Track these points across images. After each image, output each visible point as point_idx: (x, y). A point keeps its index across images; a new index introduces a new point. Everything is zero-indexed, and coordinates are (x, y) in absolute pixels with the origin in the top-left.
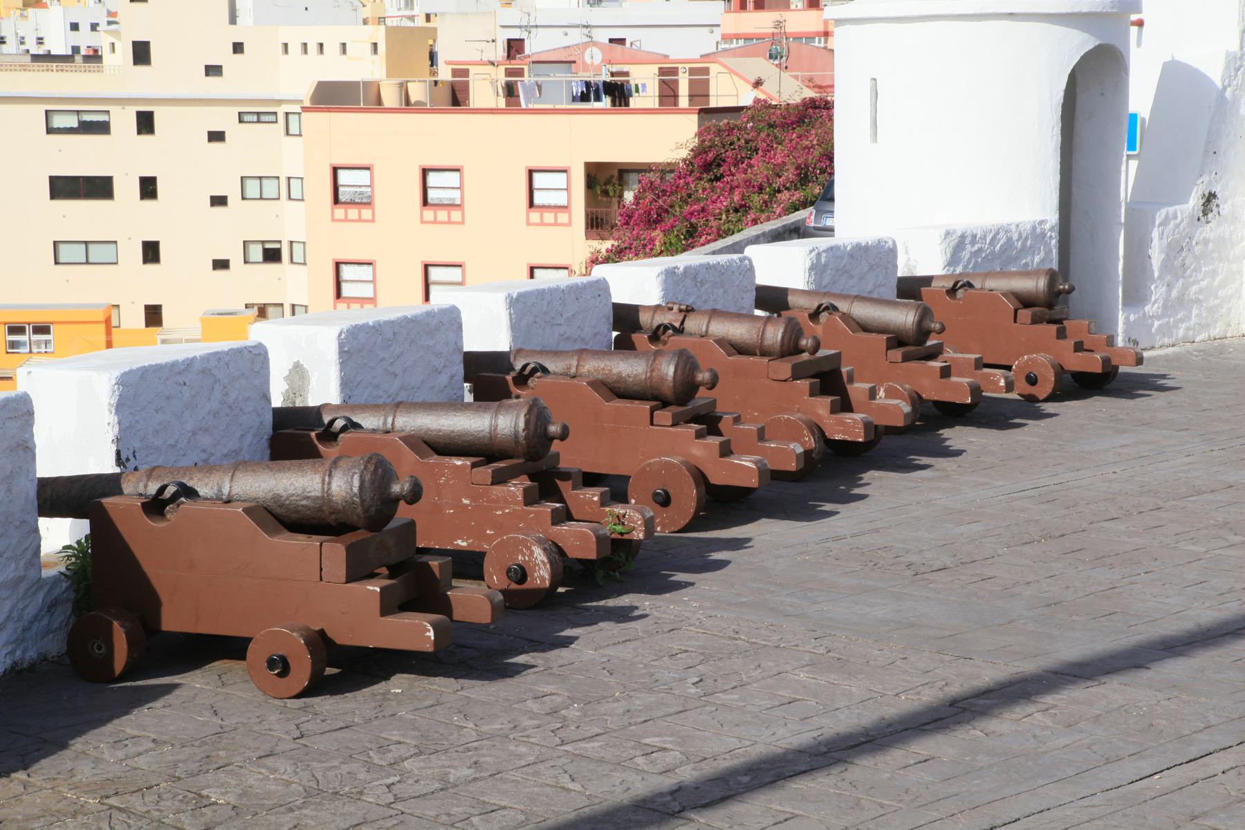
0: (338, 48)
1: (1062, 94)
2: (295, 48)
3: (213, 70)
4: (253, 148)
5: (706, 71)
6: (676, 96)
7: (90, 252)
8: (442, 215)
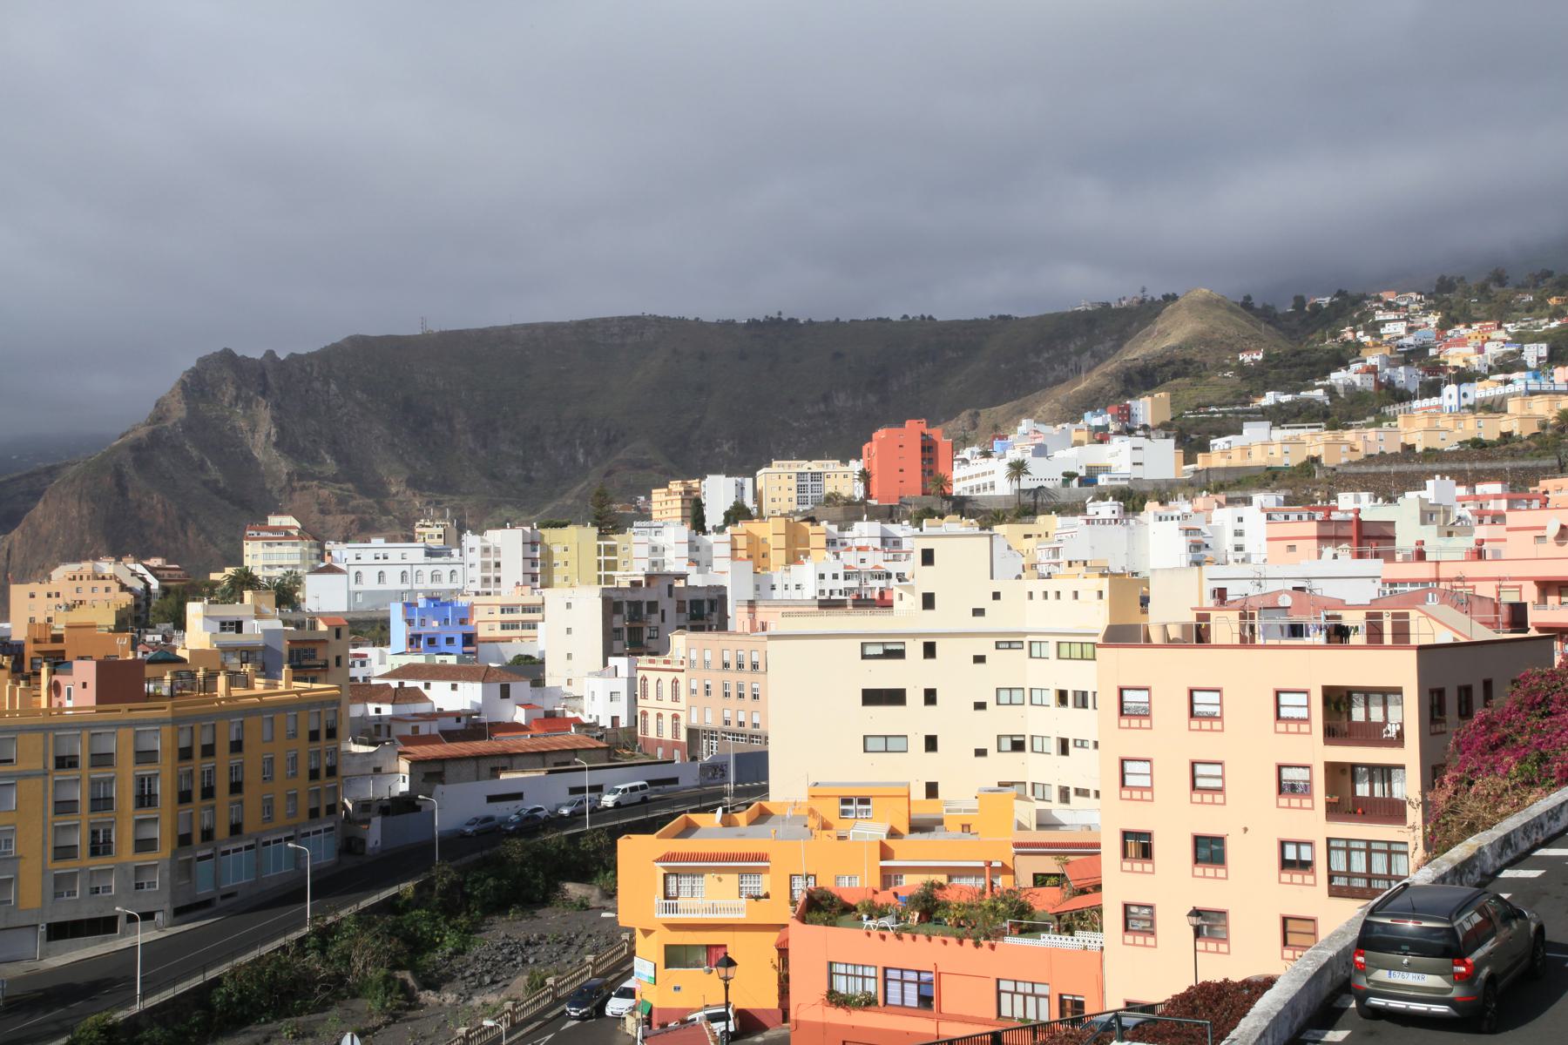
0: (1071, 595)
3: (978, 612)
4: (1007, 668)
5: (1406, 615)
6: (1381, 634)
7: (888, 744)
8: (1206, 725)
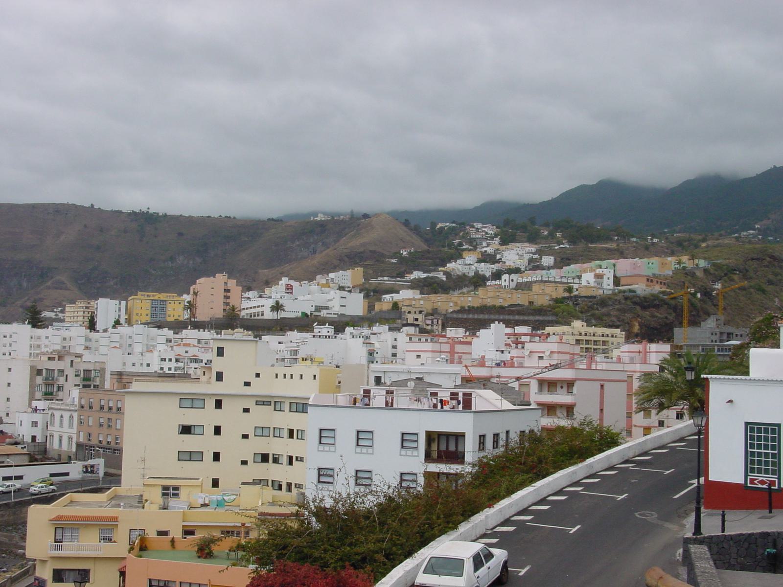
1: (565, 190)
2: (281, 376)
3: (247, 384)
